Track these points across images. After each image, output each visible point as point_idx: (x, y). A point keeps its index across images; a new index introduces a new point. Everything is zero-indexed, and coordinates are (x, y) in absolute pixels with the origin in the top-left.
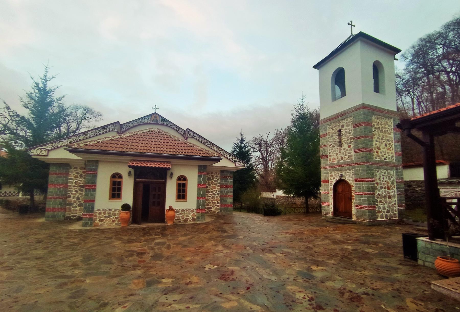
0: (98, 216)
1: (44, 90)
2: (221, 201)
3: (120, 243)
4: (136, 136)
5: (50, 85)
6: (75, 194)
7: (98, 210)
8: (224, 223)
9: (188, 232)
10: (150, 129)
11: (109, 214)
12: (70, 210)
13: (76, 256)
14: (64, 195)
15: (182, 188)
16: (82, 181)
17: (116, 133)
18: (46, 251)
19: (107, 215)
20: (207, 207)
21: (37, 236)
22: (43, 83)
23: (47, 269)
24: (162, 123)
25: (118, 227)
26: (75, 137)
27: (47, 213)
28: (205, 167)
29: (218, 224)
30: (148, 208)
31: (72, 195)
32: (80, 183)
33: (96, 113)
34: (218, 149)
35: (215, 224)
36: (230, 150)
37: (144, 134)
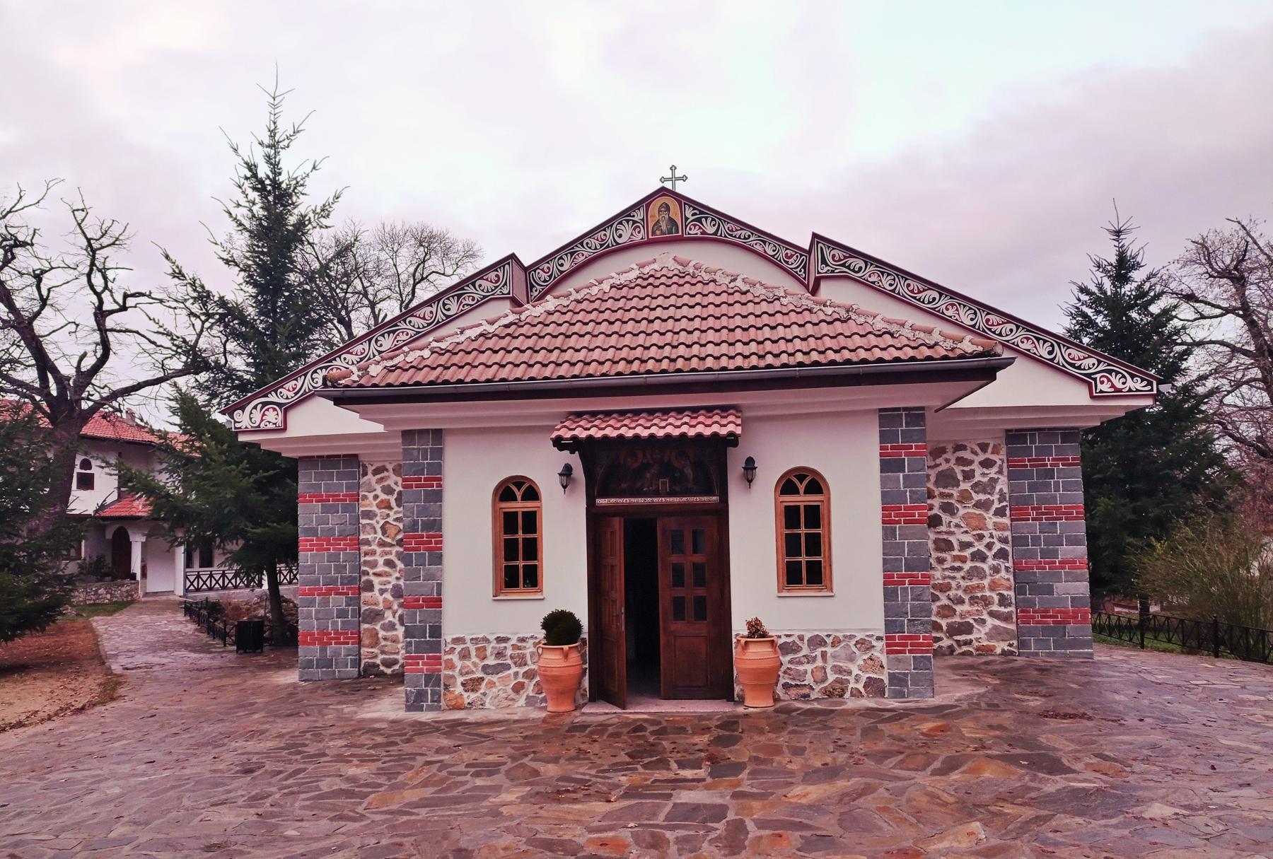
0: (458, 664)
1: (276, 185)
2: (1019, 590)
3: (523, 799)
4: (585, 305)
5: (291, 165)
7: (457, 641)
8: (1045, 714)
9: (842, 757)
10: (642, 266)
11: (499, 656)
14: (351, 580)
15: (803, 531)
17: (507, 304)
18: (250, 815)
19: (491, 661)
20: (944, 623)
21: (251, 746)
22: (268, 159)
24: (695, 232)
26: (366, 346)
27: (302, 649)
28: (916, 415)
29: (1006, 718)
30: (653, 622)
31: (376, 580)
33: (460, 248)
34: (981, 319)
35: (993, 718)
36: (1060, 324)
37: (618, 294)
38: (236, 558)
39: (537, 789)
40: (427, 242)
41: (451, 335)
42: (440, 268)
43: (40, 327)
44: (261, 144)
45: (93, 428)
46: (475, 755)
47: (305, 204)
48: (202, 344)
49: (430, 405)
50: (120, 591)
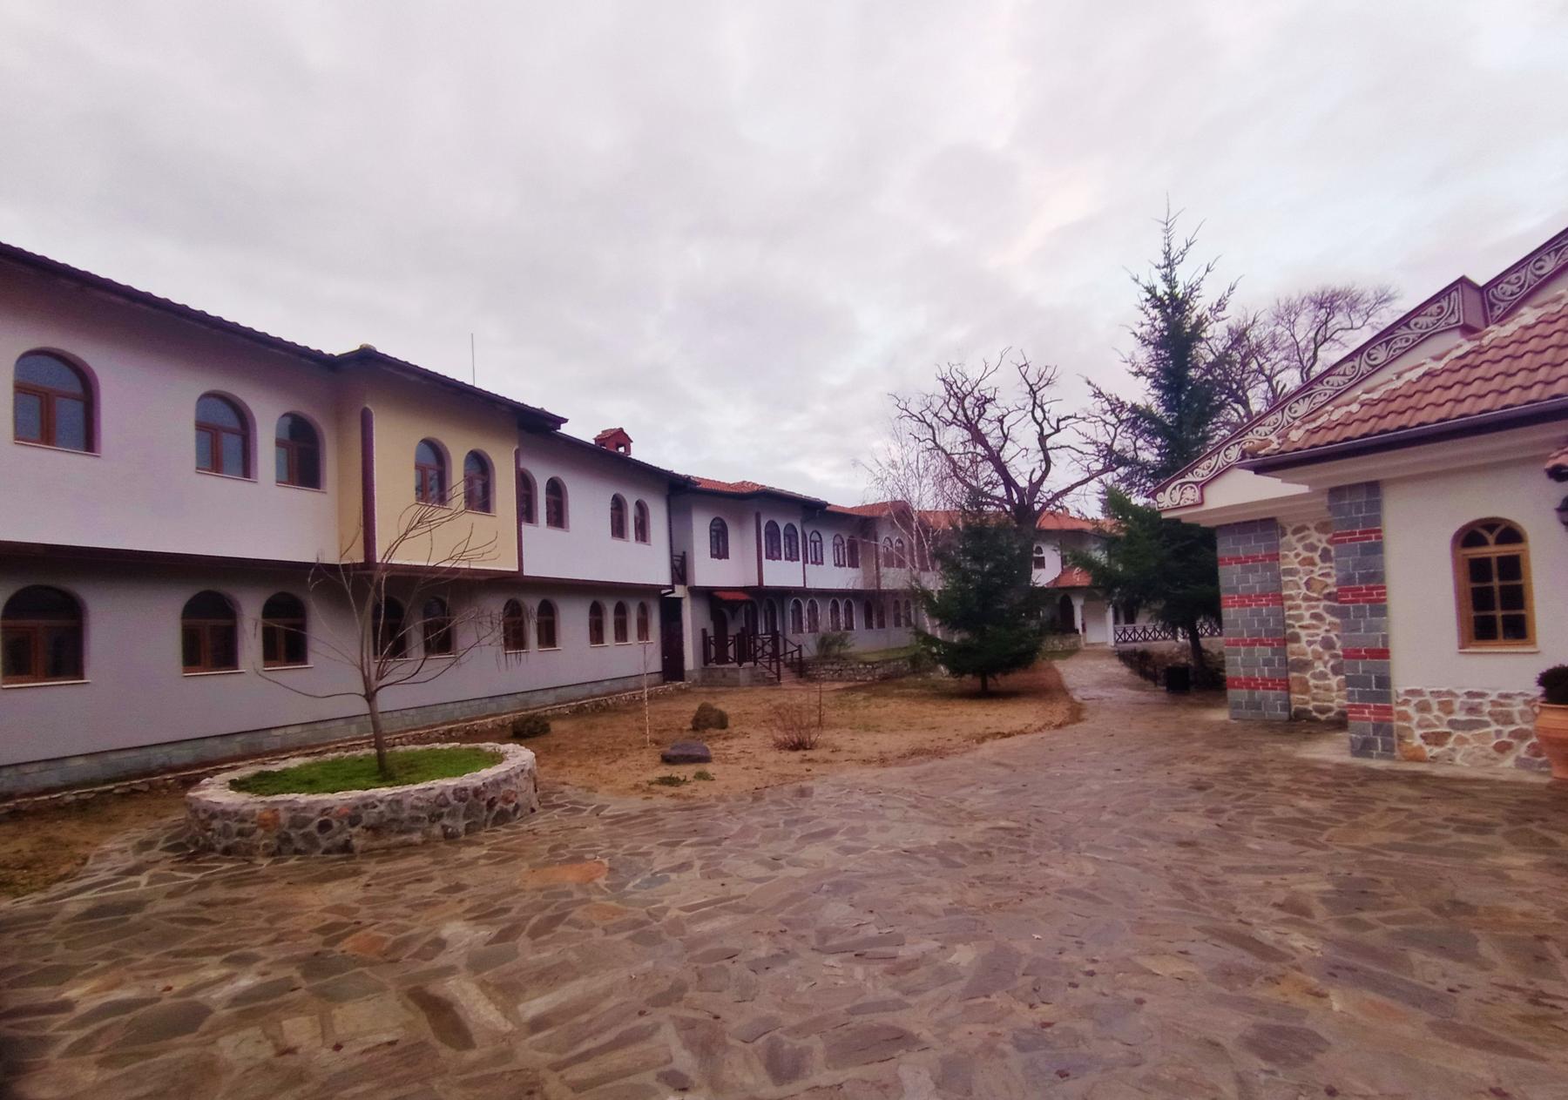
1: (1173, 297)
3: (1537, 867)
5: (1184, 276)
6: (1314, 632)
11: (1476, 712)
12: (1305, 688)
13: (1307, 870)
14: (1276, 632)
16: (1328, 575)
18: (1211, 824)
19: (1461, 716)
21: (1198, 768)
22: (1165, 278)
23: (1202, 892)
25: (1531, 778)
26: (1279, 416)
27: (1231, 693)
31: (1303, 633)
32: (1327, 586)
38: (1159, 615)
39: (1559, 860)
40: (1328, 303)
41: (1386, 382)
42: (1347, 324)
43: (1006, 455)
44: (1158, 267)
45: (1047, 523)
46: (1452, 810)
47: (1201, 306)
48: (1117, 447)
49: (1358, 463)
50: (1069, 642)
